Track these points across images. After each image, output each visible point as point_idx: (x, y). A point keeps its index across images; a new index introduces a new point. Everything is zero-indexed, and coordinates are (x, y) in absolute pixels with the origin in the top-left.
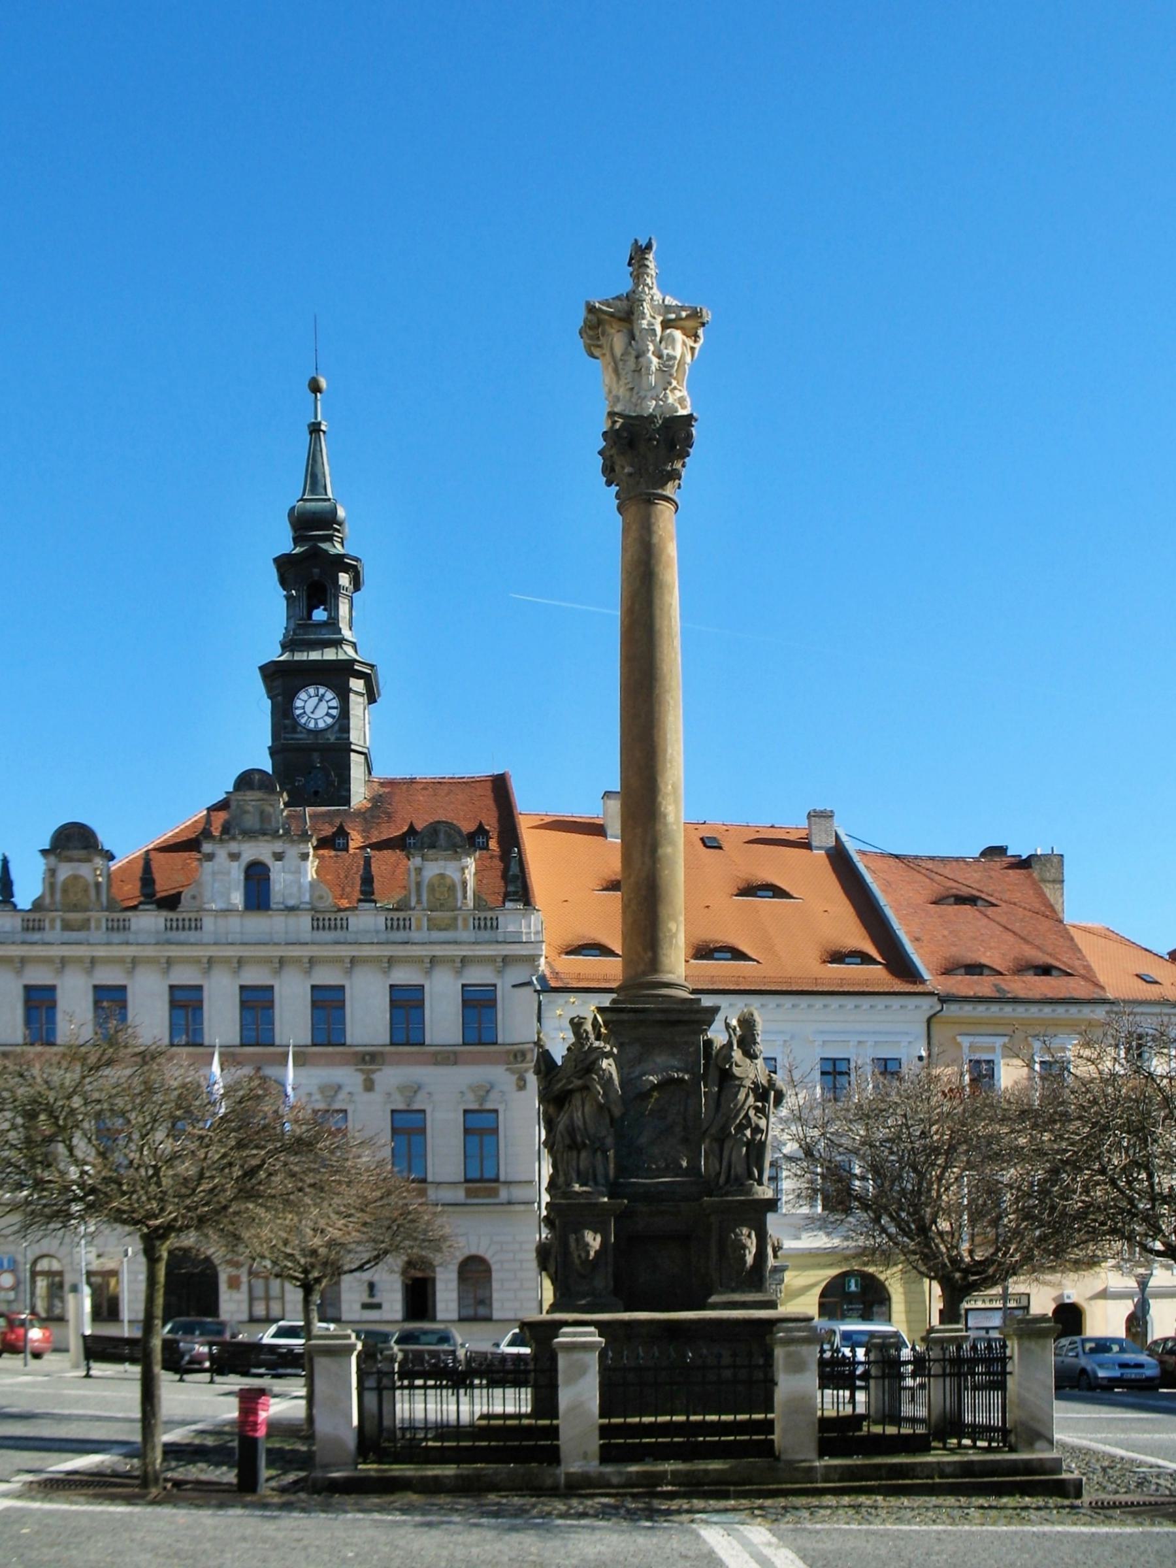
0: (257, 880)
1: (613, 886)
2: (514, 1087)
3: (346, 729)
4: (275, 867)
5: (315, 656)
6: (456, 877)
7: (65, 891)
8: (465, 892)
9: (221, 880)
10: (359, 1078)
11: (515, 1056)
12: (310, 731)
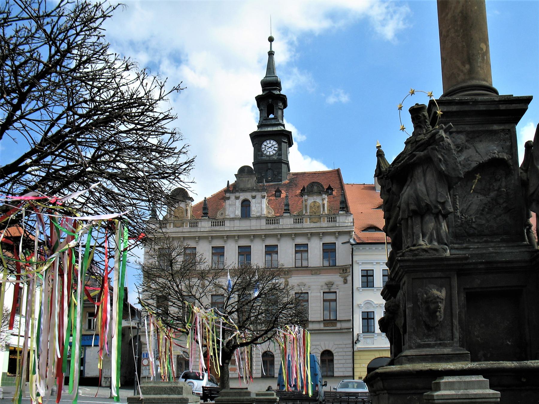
0: (246, 204)
1: (379, 207)
2: (342, 283)
3: (280, 155)
4: (253, 202)
5: (270, 129)
6: (320, 202)
8: (324, 208)
9: (233, 208)
11: (343, 270)
12: (267, 156)
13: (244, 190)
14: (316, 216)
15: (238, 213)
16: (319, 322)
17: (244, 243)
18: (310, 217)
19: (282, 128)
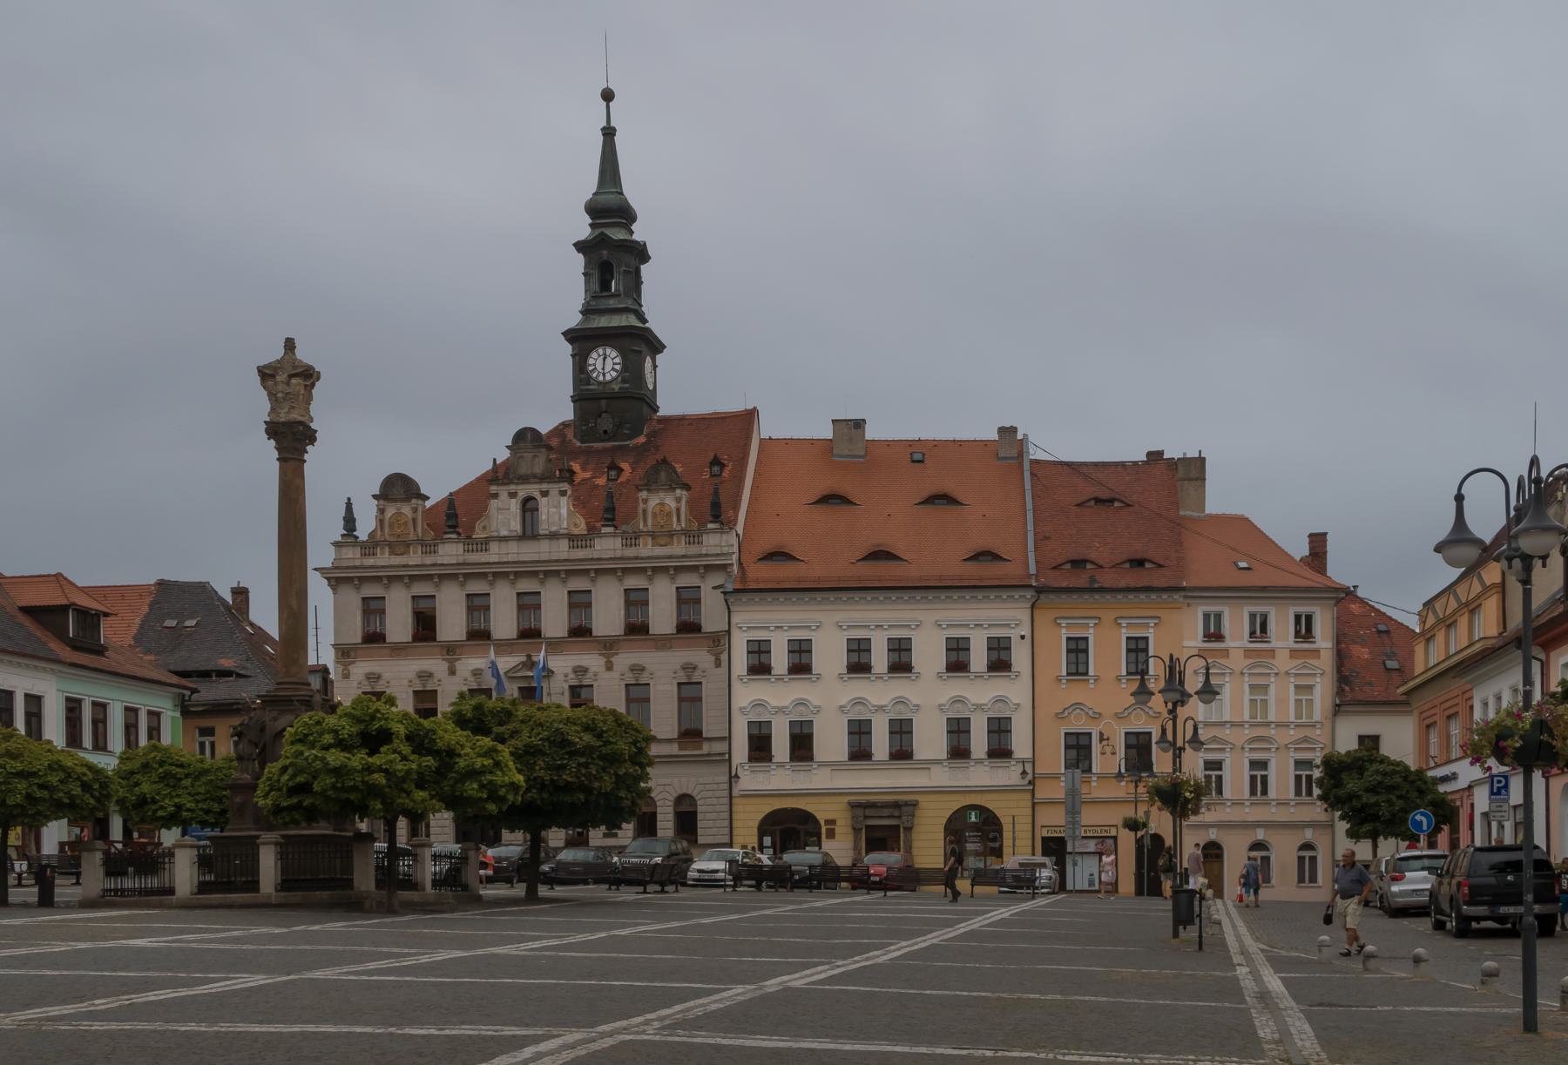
4: (543, 501)
7: (391, 525)
10: (602, 661)
13: (524, 479)
14: (663, 535)
15: (516, 526)
16: (669, 741)
17: (526, 585)
18: (653, 535)
19: (633, 321)
